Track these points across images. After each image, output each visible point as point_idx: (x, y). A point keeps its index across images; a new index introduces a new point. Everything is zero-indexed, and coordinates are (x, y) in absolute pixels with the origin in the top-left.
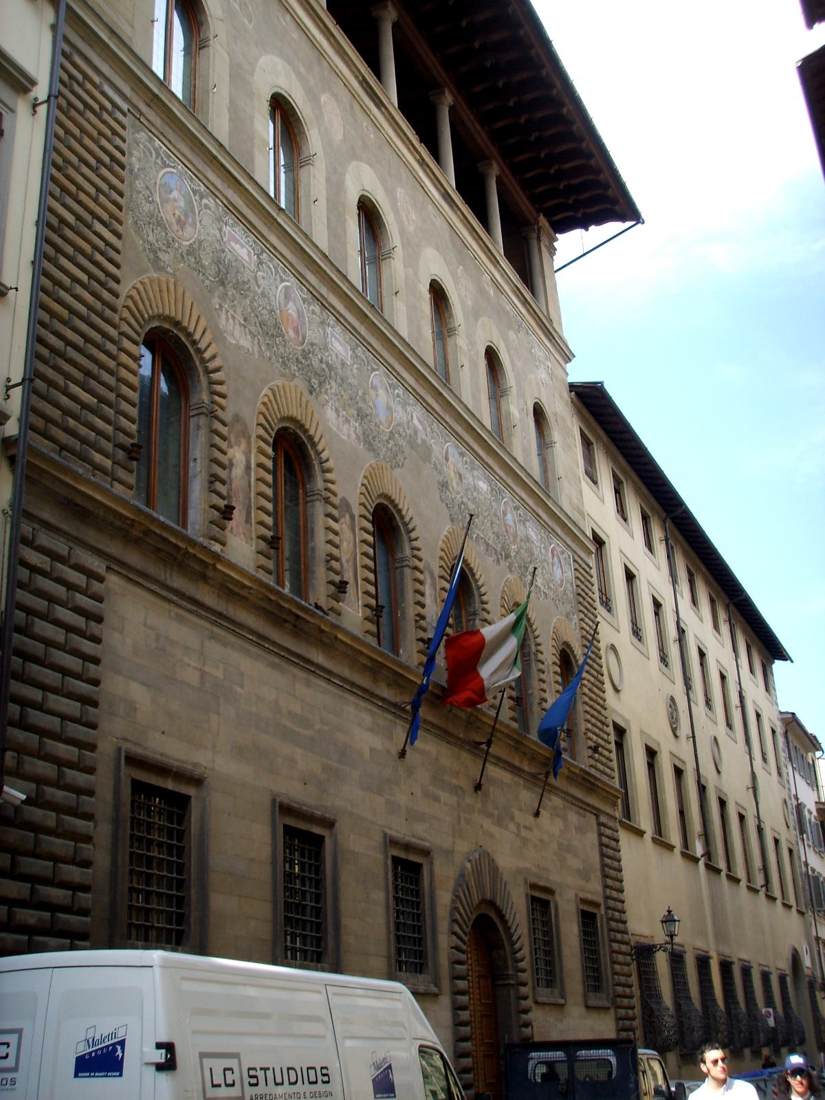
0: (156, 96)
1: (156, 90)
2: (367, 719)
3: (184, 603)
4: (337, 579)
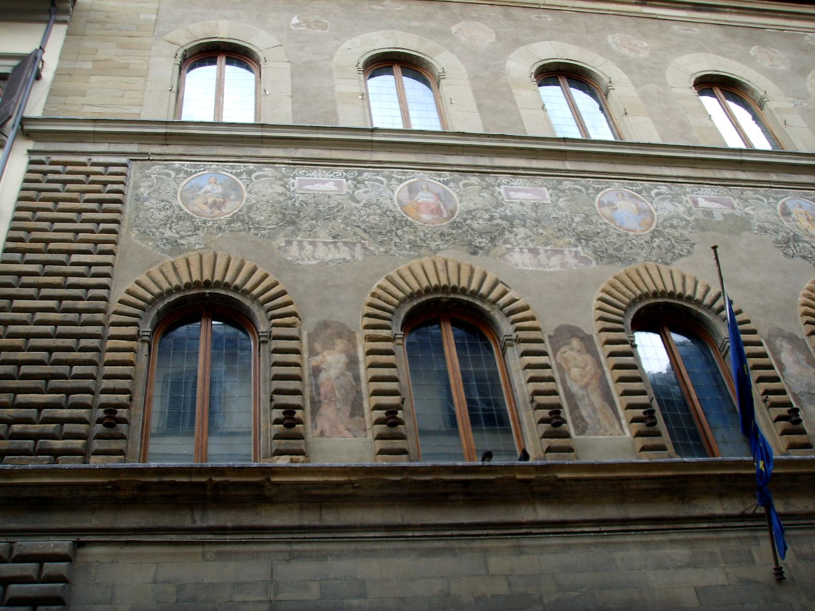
0: (166, 134)
1: (163, 131)
2: (681, 553)
3: (228, 537)
4: (784, 411)
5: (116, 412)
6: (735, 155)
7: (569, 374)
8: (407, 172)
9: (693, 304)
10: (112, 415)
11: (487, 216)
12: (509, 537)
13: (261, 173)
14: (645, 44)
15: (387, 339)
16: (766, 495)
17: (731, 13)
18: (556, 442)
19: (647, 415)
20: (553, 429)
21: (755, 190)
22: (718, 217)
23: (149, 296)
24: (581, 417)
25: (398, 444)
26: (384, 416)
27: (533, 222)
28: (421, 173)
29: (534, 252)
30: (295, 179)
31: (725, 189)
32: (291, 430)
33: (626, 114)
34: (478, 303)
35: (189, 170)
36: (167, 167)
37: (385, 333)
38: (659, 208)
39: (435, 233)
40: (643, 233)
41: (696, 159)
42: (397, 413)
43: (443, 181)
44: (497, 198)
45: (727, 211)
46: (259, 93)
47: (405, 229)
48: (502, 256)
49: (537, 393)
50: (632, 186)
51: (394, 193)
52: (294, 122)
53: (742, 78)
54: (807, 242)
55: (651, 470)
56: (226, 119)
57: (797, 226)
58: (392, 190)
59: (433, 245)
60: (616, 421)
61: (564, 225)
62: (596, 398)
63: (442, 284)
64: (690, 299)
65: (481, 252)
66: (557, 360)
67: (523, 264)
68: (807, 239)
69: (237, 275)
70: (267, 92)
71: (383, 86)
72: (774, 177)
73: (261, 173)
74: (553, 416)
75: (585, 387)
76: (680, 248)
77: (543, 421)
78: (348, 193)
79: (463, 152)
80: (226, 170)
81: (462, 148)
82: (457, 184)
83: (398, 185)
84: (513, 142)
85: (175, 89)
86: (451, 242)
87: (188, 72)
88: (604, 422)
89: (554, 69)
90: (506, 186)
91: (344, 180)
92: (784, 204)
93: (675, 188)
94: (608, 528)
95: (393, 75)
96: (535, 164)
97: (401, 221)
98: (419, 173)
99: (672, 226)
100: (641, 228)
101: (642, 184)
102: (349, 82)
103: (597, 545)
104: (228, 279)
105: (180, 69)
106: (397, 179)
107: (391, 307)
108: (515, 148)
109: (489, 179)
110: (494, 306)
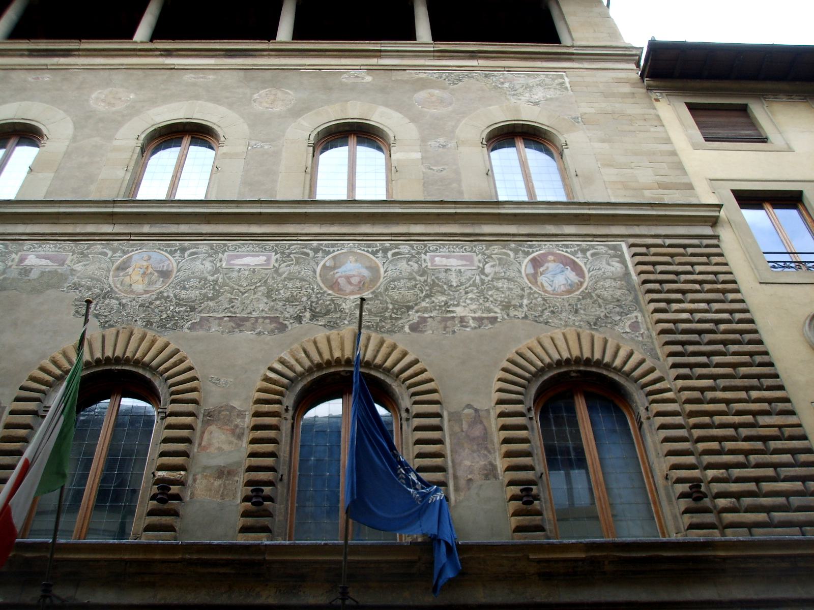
5: (170, 489)
6: (106, 207)
10: (166, 492)
13: (397, 250)
15: (521, 415)
17: (269, 56)
18: (698, 518)
19: (254, 494)
20: (254, 508)
22: (34, 275)
31: (72, 244)
32: (530, 507)
33: (577, 175)
35: (327, 249)
42: (700, 486)
43: (372, 250)
46: (391, 170)
49: (675, 467)
50: (567, 248)
54: (117, 299)
58: (519, 263)
63: (565, 358)
64: (598, 363)
71: (505, 159)
72: (146, 229)
73: (397, 250)
78: (479, 267)
80: (363, 248)
83: (525, 258)
85: (309, 170)
87: (322, 152)
92: (131, 257)
95: (515, 147)
102: (473, 153)
104: (129, 354)
105: (143, 150)
106: (524, 252)
109: (83, 245)
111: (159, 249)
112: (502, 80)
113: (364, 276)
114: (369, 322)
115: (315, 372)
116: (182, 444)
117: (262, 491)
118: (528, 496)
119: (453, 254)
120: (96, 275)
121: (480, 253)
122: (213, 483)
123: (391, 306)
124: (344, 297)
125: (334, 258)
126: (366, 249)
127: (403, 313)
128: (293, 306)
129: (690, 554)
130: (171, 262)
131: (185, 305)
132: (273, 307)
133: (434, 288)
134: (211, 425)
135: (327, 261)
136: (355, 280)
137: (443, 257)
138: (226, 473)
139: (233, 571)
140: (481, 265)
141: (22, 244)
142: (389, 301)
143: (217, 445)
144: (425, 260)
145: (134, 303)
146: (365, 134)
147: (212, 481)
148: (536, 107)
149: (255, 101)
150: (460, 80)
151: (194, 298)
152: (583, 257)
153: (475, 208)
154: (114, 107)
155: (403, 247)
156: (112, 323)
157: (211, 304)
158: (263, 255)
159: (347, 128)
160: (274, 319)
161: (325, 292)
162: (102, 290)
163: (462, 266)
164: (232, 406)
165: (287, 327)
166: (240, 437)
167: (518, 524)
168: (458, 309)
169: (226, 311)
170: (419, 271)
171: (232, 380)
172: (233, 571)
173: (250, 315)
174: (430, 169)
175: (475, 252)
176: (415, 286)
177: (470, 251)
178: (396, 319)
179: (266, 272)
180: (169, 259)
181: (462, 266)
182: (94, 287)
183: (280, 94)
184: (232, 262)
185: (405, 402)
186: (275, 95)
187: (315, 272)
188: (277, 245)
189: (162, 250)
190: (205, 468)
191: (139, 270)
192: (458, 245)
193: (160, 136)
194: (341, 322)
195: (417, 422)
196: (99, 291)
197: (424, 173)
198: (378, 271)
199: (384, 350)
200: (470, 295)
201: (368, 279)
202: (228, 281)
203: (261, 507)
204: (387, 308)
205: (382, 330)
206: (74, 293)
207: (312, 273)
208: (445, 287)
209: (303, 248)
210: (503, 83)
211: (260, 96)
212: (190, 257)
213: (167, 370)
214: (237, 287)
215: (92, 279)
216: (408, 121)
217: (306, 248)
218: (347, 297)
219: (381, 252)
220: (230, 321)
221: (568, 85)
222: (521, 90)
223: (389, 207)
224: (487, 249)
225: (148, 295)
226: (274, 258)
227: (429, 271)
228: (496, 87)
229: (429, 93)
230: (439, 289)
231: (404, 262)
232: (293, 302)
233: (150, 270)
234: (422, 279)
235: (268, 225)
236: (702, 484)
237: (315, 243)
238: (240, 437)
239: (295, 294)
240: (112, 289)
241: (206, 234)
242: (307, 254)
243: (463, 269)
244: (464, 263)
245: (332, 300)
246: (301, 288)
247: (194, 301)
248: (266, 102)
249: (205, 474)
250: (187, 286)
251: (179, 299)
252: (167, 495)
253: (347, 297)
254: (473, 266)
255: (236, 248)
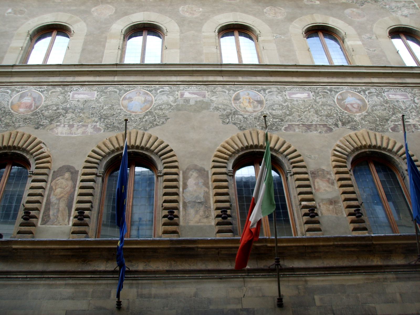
2: (69, 291)
5: (84, 213)
6: (217, 67)
7: (54, 192)
8: (24, 87)
9: (386, 151)
10: (226, 213)
11: (55, 108)
12: (329, 275)
14: (201, 10)
16: (414, 255)
20: (223, 220)
21: (224, 87)
22: (192, 102)
23: (103, 154)
24: (49, 216)
25: (362, 225)
26: (308, 212)
27: (79, 110)
28: (32, 87)
29: (71, 126)
30: (178, 92)
31: (205, 87)
32: (313, 219)
34: (25, 154)
35: (235, 89)
36: (223, 88)
37: (224, 170)
38: (268, 99)
39: (22, 118)
40: (141, 113)
41: (193, 71)
43: (258, 90)
44: (66, 98)
45: (200, 98)
46: (164, 48)
47: (7, 117)
48: (52, 129)
51: (231, 97)
52: (180, 62)
53: (251, 24)
54: (241, 115)
55: (67, 245)
56: (146, 62)
57: (240, 106)
58: (231, 96)
59: (17, 125)
60: (67, 217)
61: (96, 111)
62: (62, 205)
65: (41, 127)
66: (52, 184)
67: (62, 133)
68: (242, 113)
69: (24, 144)
70: (70, 48)
71: (228, 42)
72: (240, 79)
74: (311, 212)
75: (59, 199)
76: (159, 120)
77: (305, 215)
78: (412, 100)
79: (60, 75)
81: (59, 73)
82: (48, 92)
84: (87, 68)
86: (28, 123)
87: (129, 39)
88: (60, 218)
89: (142, 27)
90: (289, 92)
91: (310, 92)
92: (238, 94)
93: (174, 88)
94: (32, 276)
96: (98, 79)
97: (7, 113)
98: (30, 87)
99: (161, 109)
100: (141, 111)
101: (155, 87)
103: (21, 285)
105: (124, 38)
107: (227, 156)
108: (88, 71)
109: (211, 87)
110: (32, 156)
111: (252, 89)
112: (384, 4)
113: (359, 104)
114: (371, 127)
115: (355, 151)
116: (306, 189)
117: (30, 213)
118: (359, 213)
119: (397, 93)
120: (225, 102)
121: (409, 93)
122: (329, 207)
123: (378, 119)
124: (354, 114)
125: (341, 94)
126: (354, 90)
127: (385, 122)
128: (331, 118)
129: (97, 247)
130: (261, 96)
131: (278, 118)
132: (321, 119)
133: (395, 110)
134: (316, 178)
135: (337, 96)
136: (355, 106)
137: (393, 94)
138: (333, 202)
139: (358, 250)
140: (412, 99)
141: (179, 87)
142: (376, 116)
143: (323, 188)
144: (385, 96)
145: (251, 117)
146: (152, 29)
147: (328, 206)
148: (406, 18)
149: (266, 13)
150: (363, 4)
151: (280, 115)
152: (264, 93)
153: (401, 70)
154: (194, 15)
155: (273, 88)
156: (244, 127)
157: (290, 117)
158: (306, 93)
159: (317, 28)
160: (325, 125)
161: (343, 112)
162: (231, 110)
163: (404, 99)
164: (322, 169)
165: (333, 129)
166: (333, 184)
167: (219, 229)
168: (410, 120)
169: (299, 121)
170: (384, 101)
171: (317, 156)
172: (358, 250)
173: (312, 123)
174: (369, 50)
175: (407, 92)
176: (385, 109)
177: (308, 91)
178: (383, 125)
179: (311, 101)
180: (259, 95)
181: (404, 99)
182: (226, 109)
183: (277, 10)
184: (292, 96)
185: (160, 166)
186: (275, 10)
187: (334, 101)
188: (310, 88)
189: (253, 90)
190: (322, 200)
191: (136, 100)
192: (397, 89)
193: (222, 31)
194: (358, 127)
195: (34, 177)
196: (230, 111)
197: (367, 52)
198: (364, 101)
199: (151, 141)
200: (413, 114)
201: (361, 105)
202: (293, 106)
203: (28, 221)
204: (377, 120)
205: (379, 131)
206: (217, 112)
207: (333, 102)
208: (400, 109)
209: (323, 90)
210: (385, 6)
211: (267, 10)
212: (269, 94)
213: (284, 151)
214: (299, 109)
215: (224, 105)
216: (348, 25)
217: (325, 89)
218: (355, 114)
219: (262, 91)
220: (303, 126)
221: (417, 6)
222: (395, 9)
223: (360, 69)
224: (412, 91)
225: (256, 113)
226: (311, 94)
227: (389, 102)
228: (382, 8)
229: (351, 10)
230: (398, 110)
231: (375, 97)
232: (330, 117)
233: (251, 101)
234: (388, 105)
235: (302, 78)
236: (316, 209)
237: (329, 87)
238: (333, 184)
239: (329, 113)
240: (236, 110)
241: (273, 82)
242: (327, 93)
243: (405, 100)
244: (404, 97)
245: (348, 116)
246: (331, 110)
247: (281, 116)
248: (272, 14)
249: (323, 203)
250: (274, 109)
251: (273, 115)
252: (312, 214)
253: (355, 114)
254: (409, 99)
255: (290, 90)
